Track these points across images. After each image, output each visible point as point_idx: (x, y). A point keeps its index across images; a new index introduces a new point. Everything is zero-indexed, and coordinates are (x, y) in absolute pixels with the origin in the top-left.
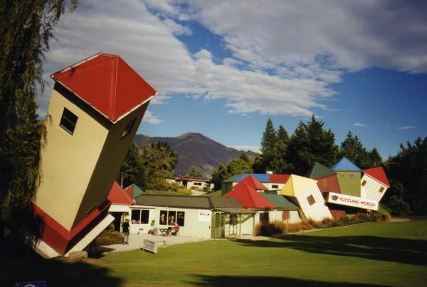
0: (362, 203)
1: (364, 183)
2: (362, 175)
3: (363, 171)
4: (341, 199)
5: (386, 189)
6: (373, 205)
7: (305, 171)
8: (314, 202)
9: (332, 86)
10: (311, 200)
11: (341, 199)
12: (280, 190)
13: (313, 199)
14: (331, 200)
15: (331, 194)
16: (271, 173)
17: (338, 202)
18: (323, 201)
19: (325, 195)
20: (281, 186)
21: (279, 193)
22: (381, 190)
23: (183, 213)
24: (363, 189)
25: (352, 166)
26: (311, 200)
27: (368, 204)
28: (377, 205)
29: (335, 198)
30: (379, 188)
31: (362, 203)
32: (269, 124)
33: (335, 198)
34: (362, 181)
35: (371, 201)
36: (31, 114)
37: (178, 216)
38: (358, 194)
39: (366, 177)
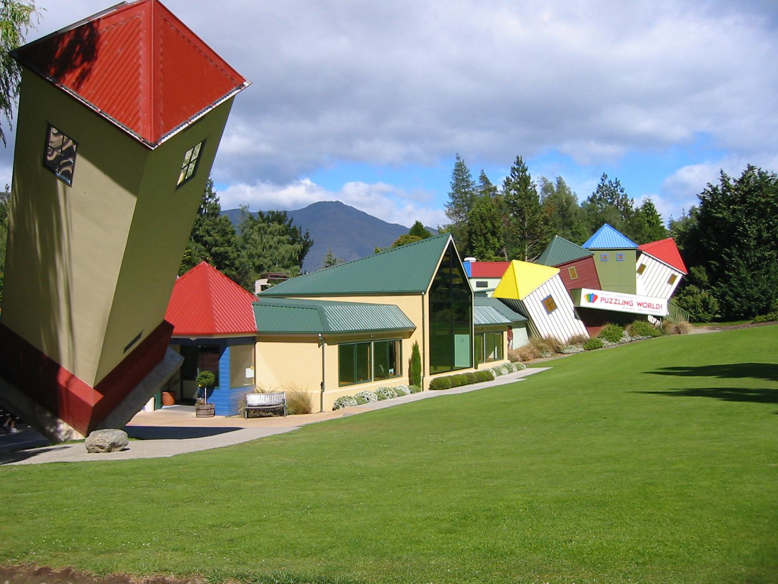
0: (639, 304)
1: (642, 268)
2: (639, 253)
3: (640, 247)
4: (602, 299)
5: (679, 277)
6: (659, 307)
7: (536, 255)
8: (556, 307)
9: (130, 580)
10: (549, 304)
11: (602, 299)
12: (493, 290)
13: (546, 307)
14: (584, 303)
15: (585, 292)
16: (473, 259)
17: (598, 305)
18: (571, 306)
19: (574, 294)
20: (492, 283)
21: (490, 295)
22: (671, 280)
23: (487, 282)
24: (640, 280)
25: (622, 241)
26: (549, 304)
27: (649, 305)
28: (664, 303)
29: (593, 298)
30: (667, 276)
31: (639, 304)
32: (460, 171)
33: (593, 298)
34: (638, 265)
35: (654, 301)
36: (732, 527)
37: (268, 409)
38: (632, 290)
39: (643, 259)
